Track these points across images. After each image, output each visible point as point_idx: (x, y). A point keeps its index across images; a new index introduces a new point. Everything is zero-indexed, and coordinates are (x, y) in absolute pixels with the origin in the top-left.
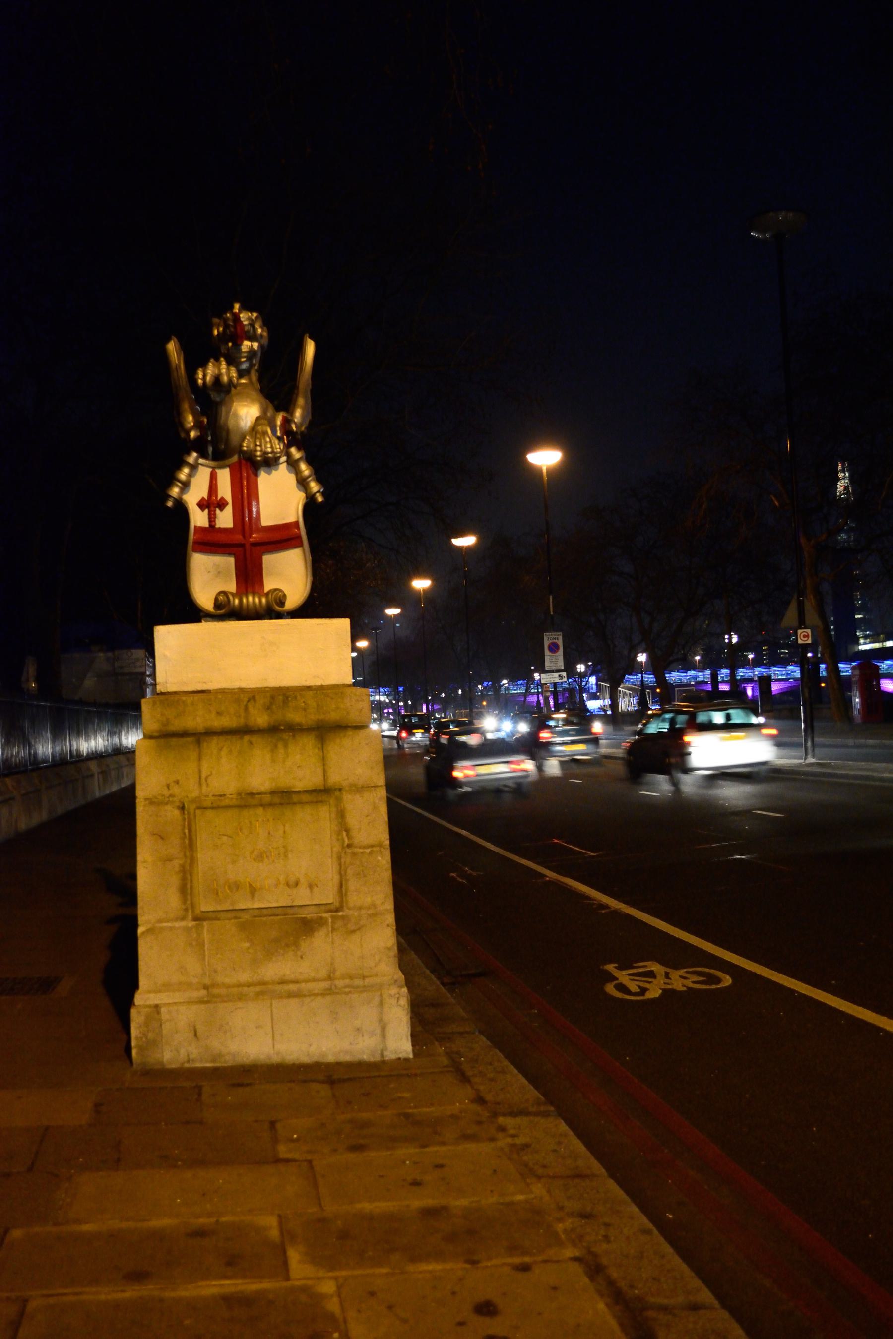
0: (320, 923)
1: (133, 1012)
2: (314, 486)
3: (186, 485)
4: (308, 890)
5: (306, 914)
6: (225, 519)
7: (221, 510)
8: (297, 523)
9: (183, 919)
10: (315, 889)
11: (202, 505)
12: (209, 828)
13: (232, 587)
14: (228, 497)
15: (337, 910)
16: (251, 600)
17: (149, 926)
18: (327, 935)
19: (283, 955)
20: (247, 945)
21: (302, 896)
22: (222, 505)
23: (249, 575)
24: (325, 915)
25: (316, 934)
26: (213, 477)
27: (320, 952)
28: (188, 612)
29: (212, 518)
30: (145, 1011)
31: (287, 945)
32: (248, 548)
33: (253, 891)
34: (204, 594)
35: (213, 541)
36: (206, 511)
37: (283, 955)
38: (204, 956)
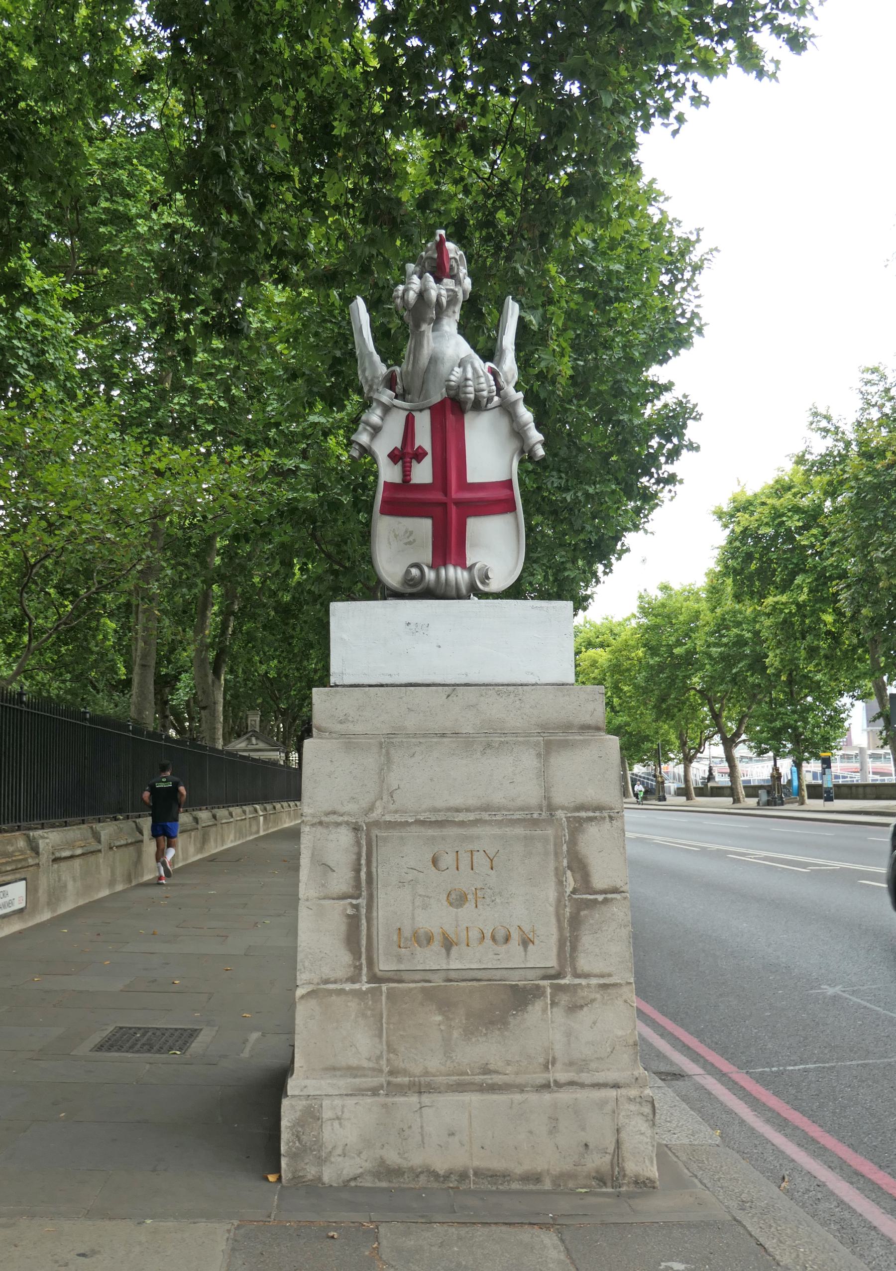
0: (536, 992)
1: (285, 1103)
2: (536, 436)
3: (376, 430)
4: (521, 948)
5: (514, 979)
6: (423, 473)
7: (419, 462)
8: (508, 484)
9: (353, 979)
10: (531, 946)
11: (395, 456)
12: (400, 860)
13: (426, 555)
14: (427, 446)
15: (558, 976)
16: (454, 574)
17: (309, 988)
18: (544, 1011)
19: (486, 1034)
20: (439, 1018)
21: (512, 957)
22: (419, 455)
23: (449, 546)
24: (542, 983)
25: (530, 1008)
26: (410, 424)
27: (542, 1028)
28: (375, 590)
29: (406, 473)
30: (302, 1104)
31: (492, 1023)
32: (448, 508)
33: (448, 944)
34: (390, 565)
35: (403, 501)
36: (400, 463)
37: (486, 1034)
38: (381, 1030)
